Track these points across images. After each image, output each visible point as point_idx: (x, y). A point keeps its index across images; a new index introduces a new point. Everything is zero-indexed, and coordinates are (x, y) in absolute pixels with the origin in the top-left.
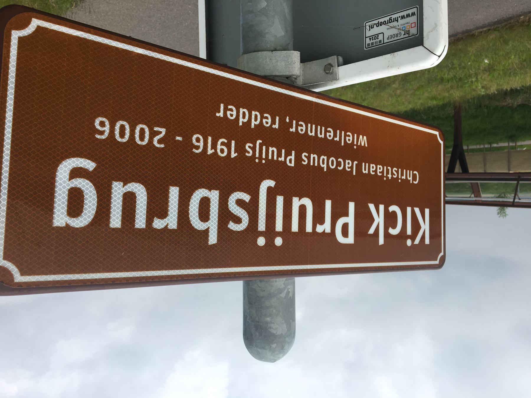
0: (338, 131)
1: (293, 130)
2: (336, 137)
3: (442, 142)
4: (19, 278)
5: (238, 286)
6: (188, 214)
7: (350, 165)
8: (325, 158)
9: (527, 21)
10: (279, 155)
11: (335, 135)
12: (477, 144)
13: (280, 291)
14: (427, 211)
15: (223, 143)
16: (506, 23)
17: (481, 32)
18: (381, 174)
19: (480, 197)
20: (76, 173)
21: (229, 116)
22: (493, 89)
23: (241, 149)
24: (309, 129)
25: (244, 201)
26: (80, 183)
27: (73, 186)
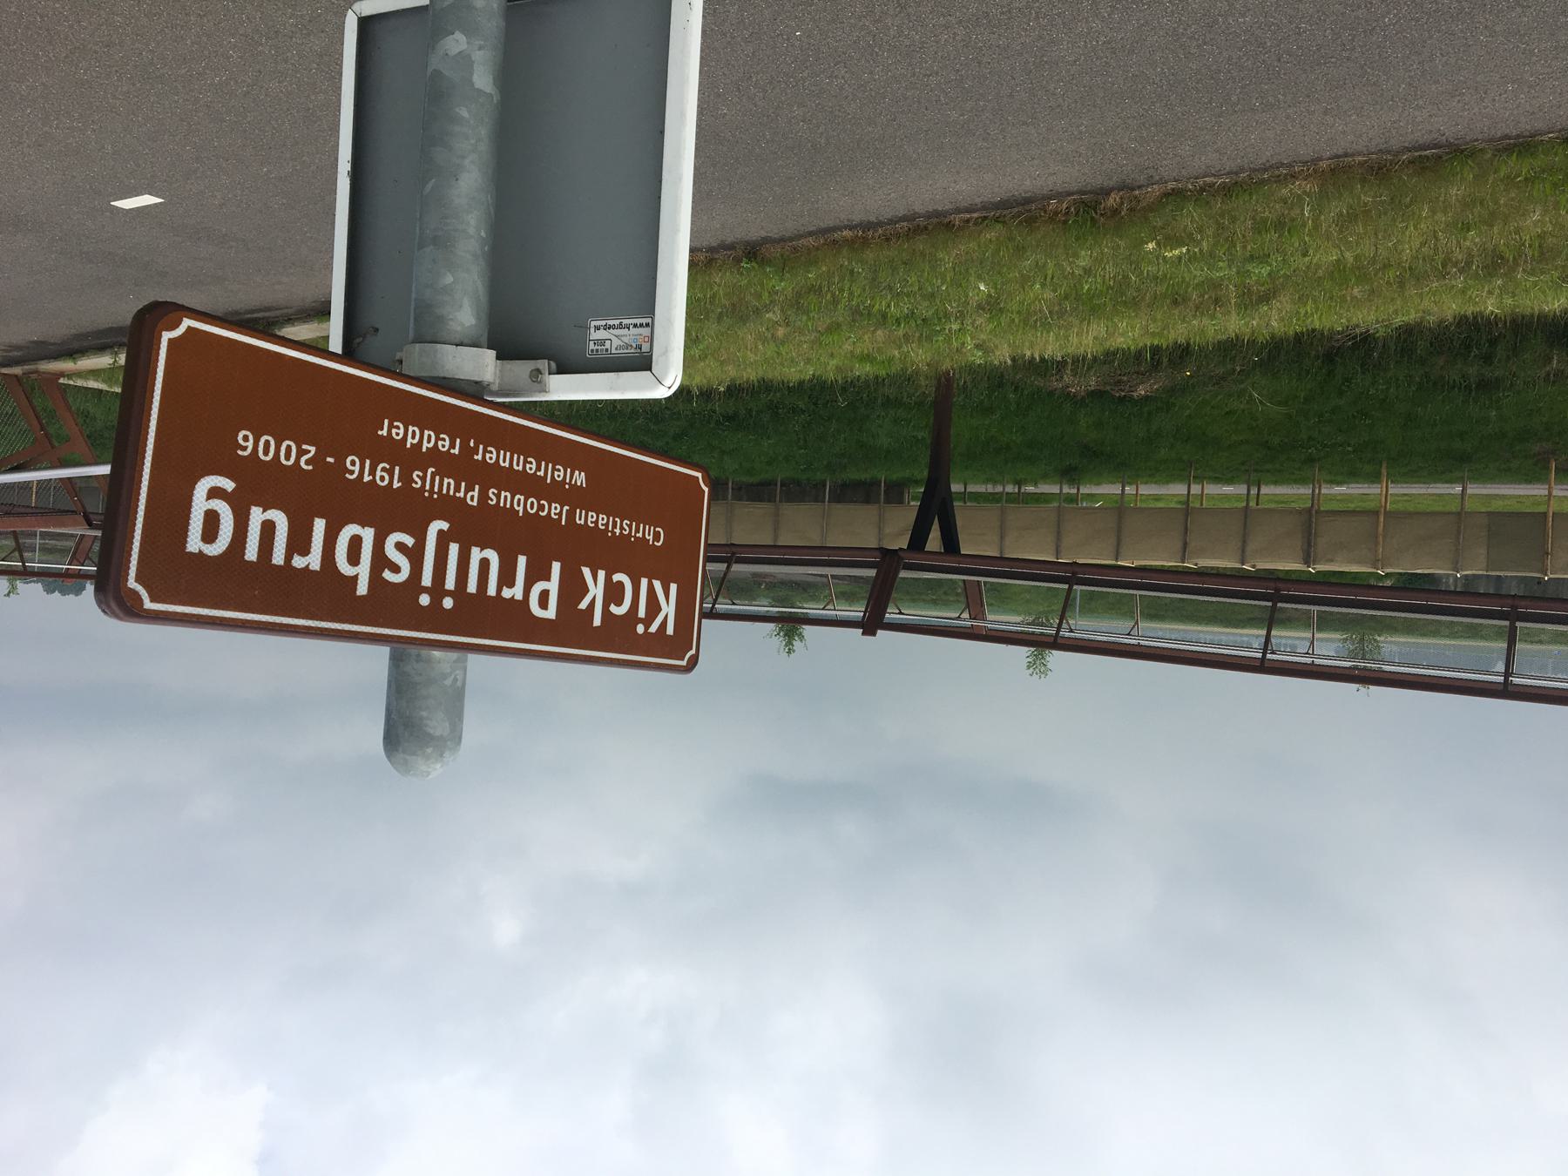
0: (543, 463)
1: (479, 457)
2: (540, 471)
3: (706, 490)
4: (148, 605)
6: (334, 554)
7: (558, 511)
8: (522, 498)
9: (1063, 212)
11: (538, 468)
12: (987, 481)
14: (673, 587)
15: (384, 469)
16: (1020, 208)
17: (968, 221)
18: (603, 527)
19: (984, 619)
20: (214, 493)
21: (394, 435)
22: (1002, 354)
23: (406, 478)
24: (501, 457)
25: (407, 545)
26: (217, 505)
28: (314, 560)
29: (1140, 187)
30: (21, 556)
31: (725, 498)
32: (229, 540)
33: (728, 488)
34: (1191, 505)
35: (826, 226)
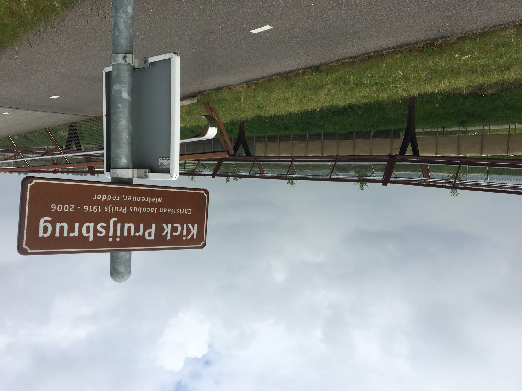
5: (109, 254)
10: (137, 230)
11: (146, 199)
12: (431, 128)
13: (123, 256)
14: (196, 225)
17: (389, 53)
20: (46, 221)
21: (98, 198)
23: (103, 209)
27: (44, 225)
28: (76, 234)
29: (449, 37)
31: (336, 139)
32: (51, 232)
33: (337, 136)
34: (511, 133)
35: (340, 58)
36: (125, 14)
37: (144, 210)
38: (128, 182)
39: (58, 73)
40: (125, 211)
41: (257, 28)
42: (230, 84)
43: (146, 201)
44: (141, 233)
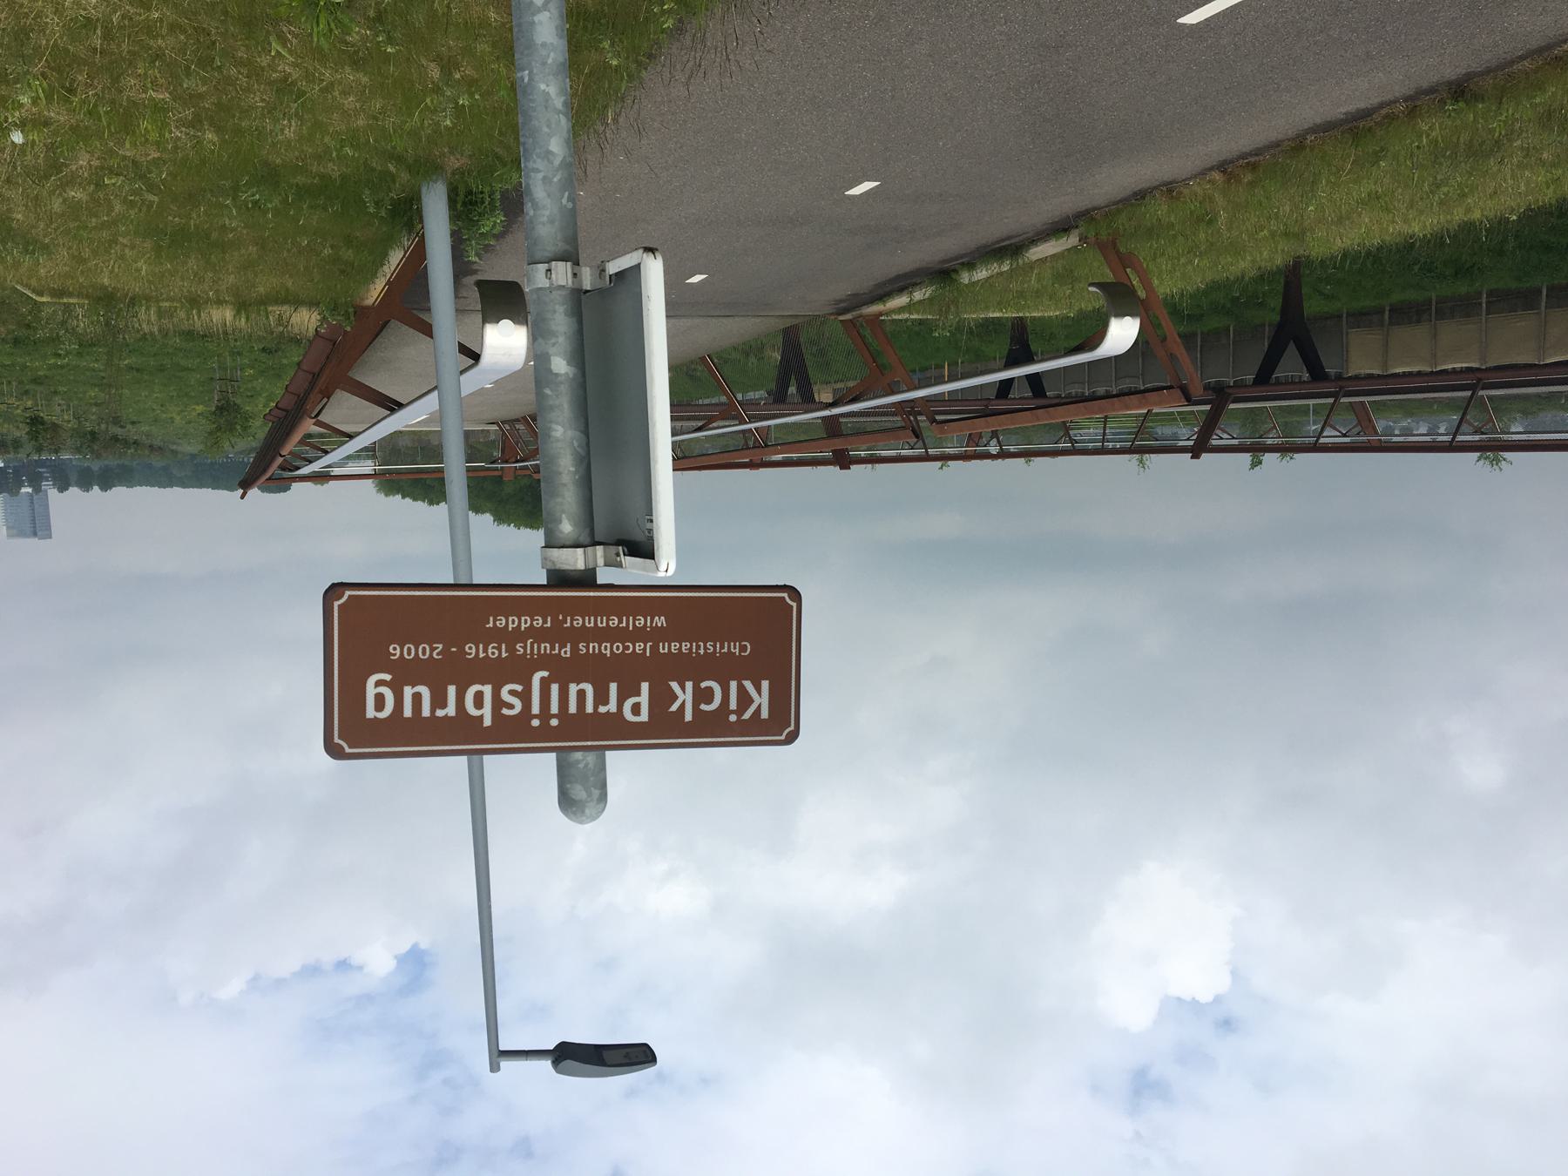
4: (348, 750)
10: (601, 698)
11: (620, 621)
13: (578, 762)
14: (765, 684)
20: (379, 683)
21: (498, 625)
28: (451, 710)
30: (924, 444)
36: (546, 162)
37: (618, 648)
38: (586, 579)
39: (686, 218)
40: (567, 652)
41: (1197, 9)
42: (1167, 177)
43: (621, 626)
44: (612, 707)
